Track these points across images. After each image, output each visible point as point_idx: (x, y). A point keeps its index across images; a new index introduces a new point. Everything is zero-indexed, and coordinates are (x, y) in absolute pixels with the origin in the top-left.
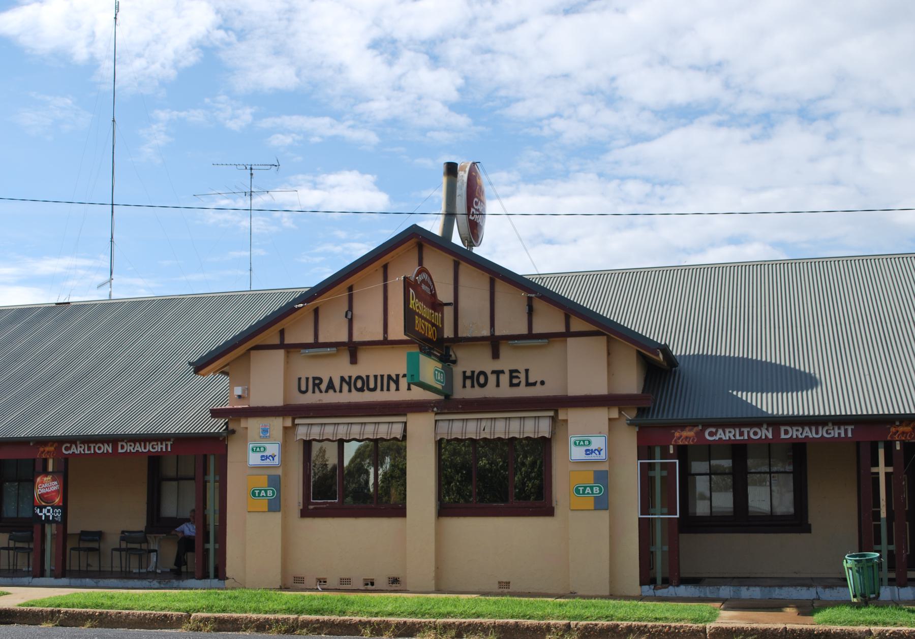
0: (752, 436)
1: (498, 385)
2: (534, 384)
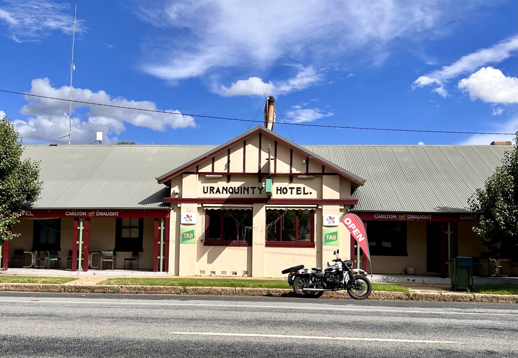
0: (390, 217)
1: (292, 193)
2: (307, 194)
